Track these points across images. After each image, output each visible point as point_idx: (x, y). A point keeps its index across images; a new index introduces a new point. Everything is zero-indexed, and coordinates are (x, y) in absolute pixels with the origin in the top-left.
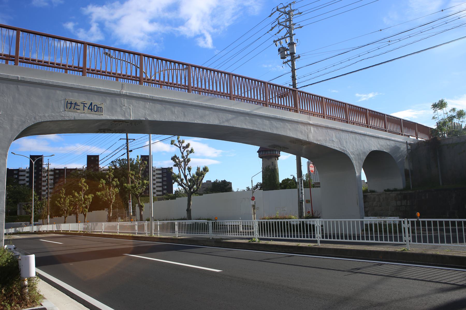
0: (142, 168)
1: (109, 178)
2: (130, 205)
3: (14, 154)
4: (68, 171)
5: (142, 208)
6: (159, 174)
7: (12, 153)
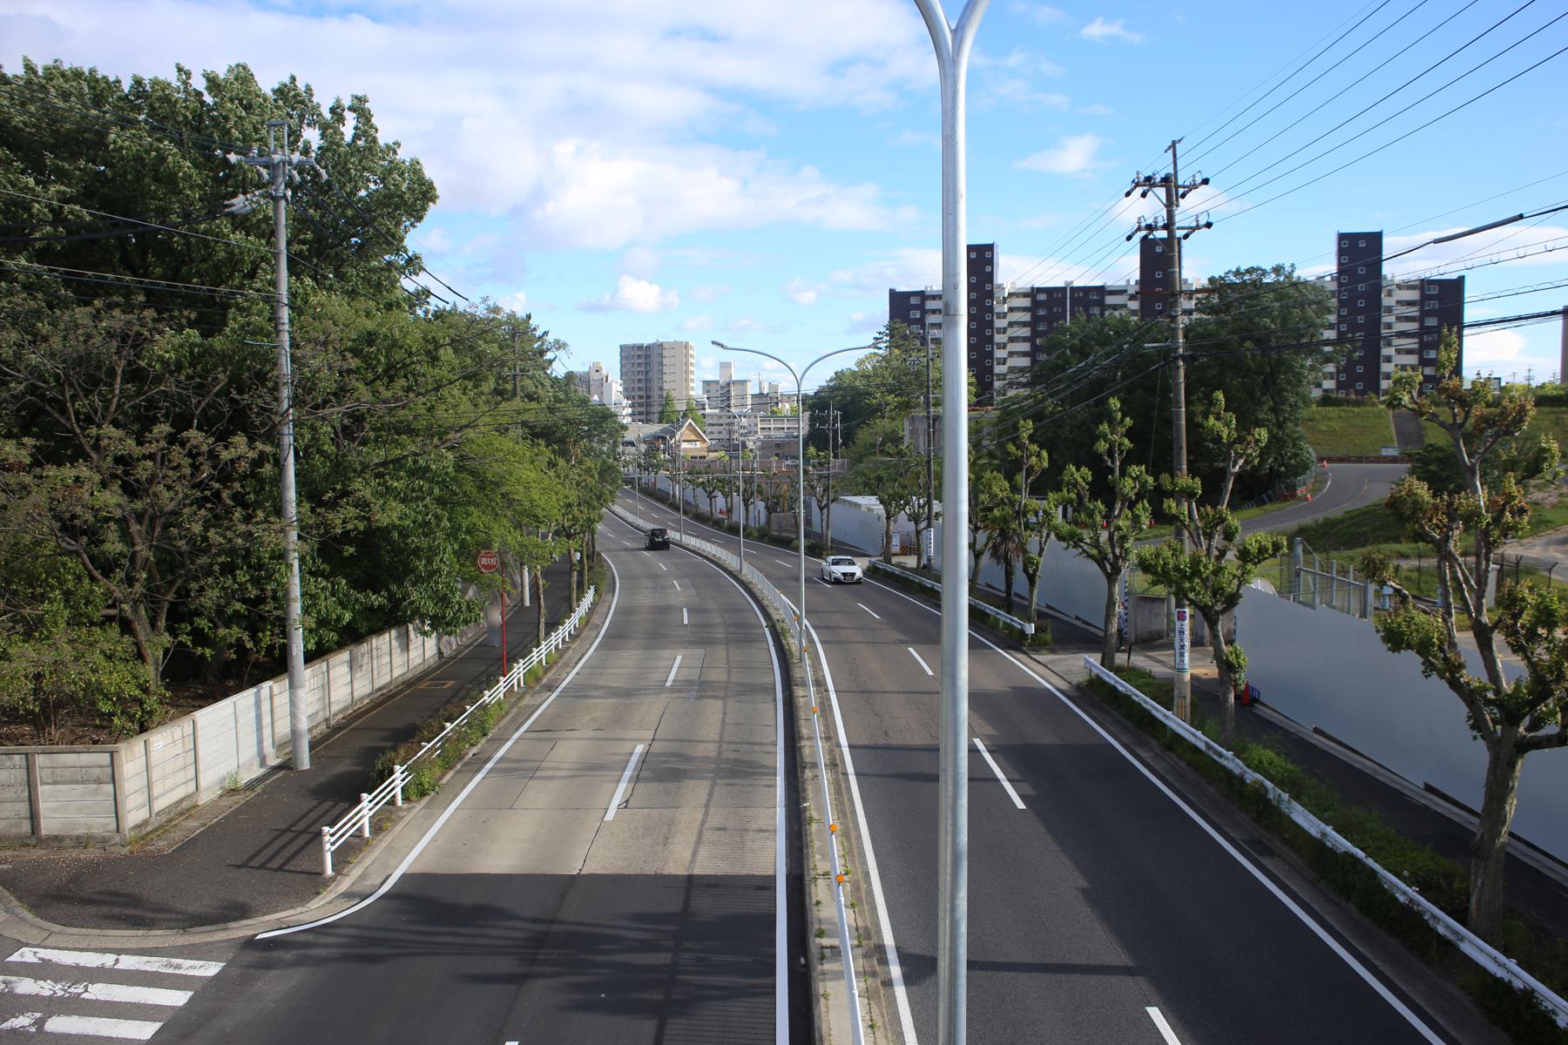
0: (1241, 462)
1: (1110, 453)
2: (1182, 632)
3: (722, 346)
4: (1076, 295)
5: (1235, 672)
6: (1410, 303)
7: (713, 343)
